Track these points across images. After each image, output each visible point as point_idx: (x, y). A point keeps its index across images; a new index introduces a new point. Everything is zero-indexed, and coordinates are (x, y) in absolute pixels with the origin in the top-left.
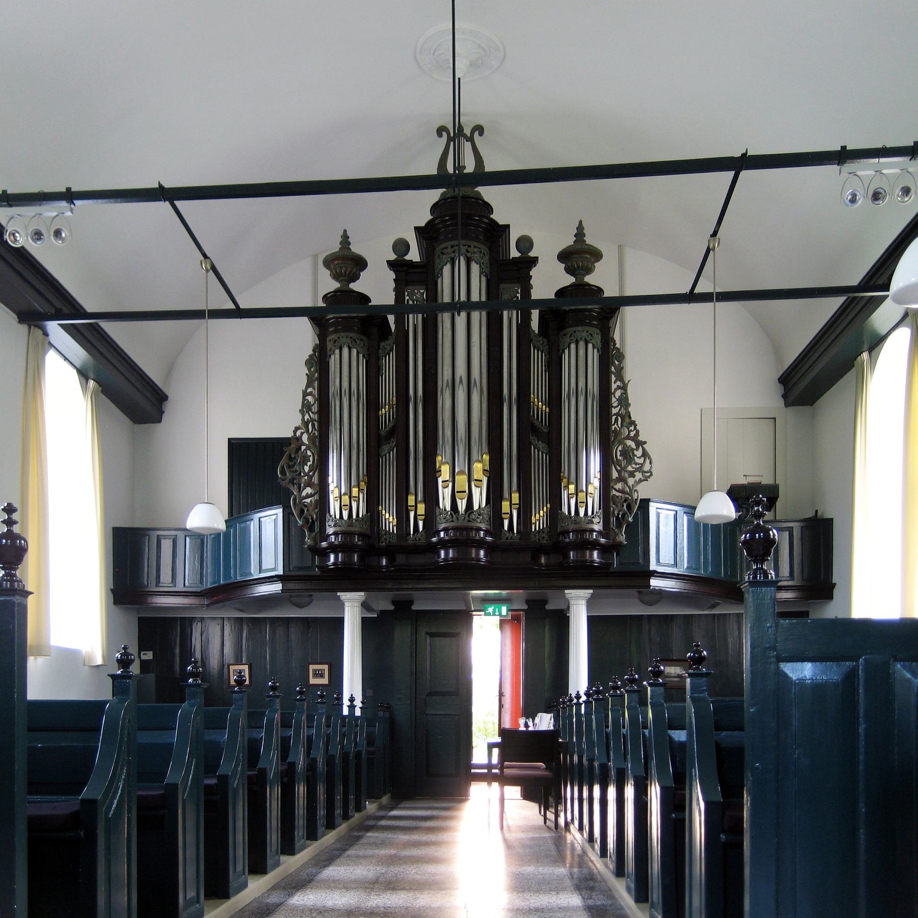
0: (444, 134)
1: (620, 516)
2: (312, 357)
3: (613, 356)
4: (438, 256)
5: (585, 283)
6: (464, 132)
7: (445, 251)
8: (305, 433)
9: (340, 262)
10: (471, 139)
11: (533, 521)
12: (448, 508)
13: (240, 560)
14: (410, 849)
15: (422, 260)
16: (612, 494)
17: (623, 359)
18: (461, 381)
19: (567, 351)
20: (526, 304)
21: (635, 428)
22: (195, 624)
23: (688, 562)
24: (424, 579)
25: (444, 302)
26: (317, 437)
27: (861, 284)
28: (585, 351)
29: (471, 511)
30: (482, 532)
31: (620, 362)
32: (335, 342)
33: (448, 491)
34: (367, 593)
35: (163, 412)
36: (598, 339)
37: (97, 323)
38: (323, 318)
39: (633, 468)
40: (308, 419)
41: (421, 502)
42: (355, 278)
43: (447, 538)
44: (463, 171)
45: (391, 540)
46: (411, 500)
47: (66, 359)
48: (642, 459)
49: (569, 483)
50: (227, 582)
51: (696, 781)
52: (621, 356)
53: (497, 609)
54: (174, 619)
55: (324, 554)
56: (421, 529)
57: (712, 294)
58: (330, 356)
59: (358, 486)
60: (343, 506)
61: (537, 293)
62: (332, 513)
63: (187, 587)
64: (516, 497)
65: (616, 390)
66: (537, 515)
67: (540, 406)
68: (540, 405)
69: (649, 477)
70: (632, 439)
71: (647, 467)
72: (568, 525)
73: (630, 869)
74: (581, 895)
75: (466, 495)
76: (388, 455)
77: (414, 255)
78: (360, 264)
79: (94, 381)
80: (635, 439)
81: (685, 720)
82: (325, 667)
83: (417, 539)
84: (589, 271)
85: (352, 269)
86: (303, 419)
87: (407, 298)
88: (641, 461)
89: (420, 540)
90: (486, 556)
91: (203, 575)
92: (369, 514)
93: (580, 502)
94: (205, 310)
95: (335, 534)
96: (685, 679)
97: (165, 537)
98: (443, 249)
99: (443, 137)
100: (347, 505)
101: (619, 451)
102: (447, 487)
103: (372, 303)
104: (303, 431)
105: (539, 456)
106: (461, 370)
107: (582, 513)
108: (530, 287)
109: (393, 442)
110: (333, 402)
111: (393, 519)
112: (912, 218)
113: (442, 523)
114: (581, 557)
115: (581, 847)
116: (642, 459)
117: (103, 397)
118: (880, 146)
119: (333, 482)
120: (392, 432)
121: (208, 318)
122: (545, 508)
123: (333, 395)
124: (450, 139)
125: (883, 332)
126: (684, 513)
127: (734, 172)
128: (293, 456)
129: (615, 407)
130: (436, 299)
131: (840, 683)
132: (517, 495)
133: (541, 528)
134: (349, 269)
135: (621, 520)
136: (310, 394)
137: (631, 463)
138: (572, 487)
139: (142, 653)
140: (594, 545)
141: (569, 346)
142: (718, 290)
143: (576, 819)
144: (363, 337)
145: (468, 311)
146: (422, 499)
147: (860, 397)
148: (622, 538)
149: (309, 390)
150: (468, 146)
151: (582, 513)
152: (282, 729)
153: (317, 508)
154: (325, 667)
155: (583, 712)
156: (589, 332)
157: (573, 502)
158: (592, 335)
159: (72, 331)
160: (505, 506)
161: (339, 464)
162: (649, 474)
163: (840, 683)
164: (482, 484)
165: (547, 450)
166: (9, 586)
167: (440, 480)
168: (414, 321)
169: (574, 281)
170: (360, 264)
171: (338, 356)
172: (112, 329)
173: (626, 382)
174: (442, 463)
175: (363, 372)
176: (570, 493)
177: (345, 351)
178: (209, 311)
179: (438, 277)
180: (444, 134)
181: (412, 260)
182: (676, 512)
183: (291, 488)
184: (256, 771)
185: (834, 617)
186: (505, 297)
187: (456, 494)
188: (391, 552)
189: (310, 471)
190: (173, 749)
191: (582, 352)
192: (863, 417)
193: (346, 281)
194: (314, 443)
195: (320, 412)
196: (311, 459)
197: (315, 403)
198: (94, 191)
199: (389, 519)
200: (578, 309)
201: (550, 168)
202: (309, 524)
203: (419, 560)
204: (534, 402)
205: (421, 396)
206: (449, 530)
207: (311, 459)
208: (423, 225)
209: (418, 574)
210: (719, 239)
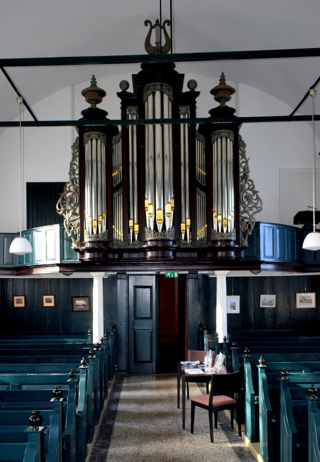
0: (149, 24)
1: (245, 231)
2: (75, 144)
3: (240, 145)
4: (145, 90)
5: (226, 106)
7: (150, 88)
11: (198, 234)
12: (152, 228)
13: (285, 245)
14: (114, 426)
15: (135, 92)
17: (245, 147)
19: (216, 143)
21: (252, 184)
22: (9, 281)
23: (280, 254)
24: (138, 265)
25: (168, 125)
26: (78, 188)
27: (189, 126)
29: (165, 230)
31: (244, 148)
32: (88, 137)
36: (232, 135)
39: (251, 205)
41: (136, 224)
42: (99, 101)
45: (120, 244)
46: (131, 223)
48: (257, 201)
49: (218, 214)
52: (244, 145)
53: (172, 274)
55: (82, 253)
56: (136, 239)
58: (85, 144)
60: (94, 226)
64: (188, 221)
65: (242, 163)
66: (200, 231)
67: (201, 172)
68: (201, 171)
69: (260, 210)
70: (251, 190)
71: (259, 205)
72: (217, 237)
73: (99, 392)
75: (162, 221)
76: (117, 198)
77: (131, 90)
78: (102, 94)
81: (35, 227)
82: (52, 297)
83: (135, 244)
84: (228, 99)
85: (98, 97)
86: (70, 178)
87: (128, 112)
88: (256, 202)
89: (136, 245)
91: (212, 425)
92: (108, 230)
93: (224, 225)
94: (19, 122)
97: (269, 257)
98: (148, 87)
99: (148, 26)
100: (162, 220)
101: (244, 196)
102: (151, 217)
104: (70, 184)
109: (121, 191)
110: (87, 164)
111: (121, 233)
113: (149, 237)
114: (19, 263)
118: (121, 110)
124: (152, 27)
126: (277, 228)
129: (241, 173)
132: (138, 226)
133: (202, 238)
134: (96, 97)
135: (245, 234)
137: (251, 203)
141: (217, 140)
143: (229, 162)
144: (104, 134)
145: (153, 124)
146: (137, 223)
147: (224, 319)
148: (246, 243)
153: (79, 227)
154: (52, 297)
155: (67, 343)
156: (228, 133)
158: (229, 134)
160: (183, 226)
161: (91, 192)
164: (171, 215)
165: (204, 195)
167: (147, 213)
168: (133, 130)
169: (220, 105)
170: (102, 94)
171: (90, 144)
172: (297, 114)
173: (247, 159)
175: (230, 149)
176: (218, 220)
177: (94, 141)
178: (22, 122)
179: (145, 102)
180: (149, 24)
182: (273, 228)
184: (94, 246)
187: (157, 221)
189: (75, 206)
192: (220, 202)
193: (94, 103)
194: (77, 192)
196: (75, 199)
197: (77, 169)
199: (119, 233)
201: (269, 294)
202: (74, 236)
204: (197, 170)
205: (220, 160)
208: (137, 73)
209: (135, 263)
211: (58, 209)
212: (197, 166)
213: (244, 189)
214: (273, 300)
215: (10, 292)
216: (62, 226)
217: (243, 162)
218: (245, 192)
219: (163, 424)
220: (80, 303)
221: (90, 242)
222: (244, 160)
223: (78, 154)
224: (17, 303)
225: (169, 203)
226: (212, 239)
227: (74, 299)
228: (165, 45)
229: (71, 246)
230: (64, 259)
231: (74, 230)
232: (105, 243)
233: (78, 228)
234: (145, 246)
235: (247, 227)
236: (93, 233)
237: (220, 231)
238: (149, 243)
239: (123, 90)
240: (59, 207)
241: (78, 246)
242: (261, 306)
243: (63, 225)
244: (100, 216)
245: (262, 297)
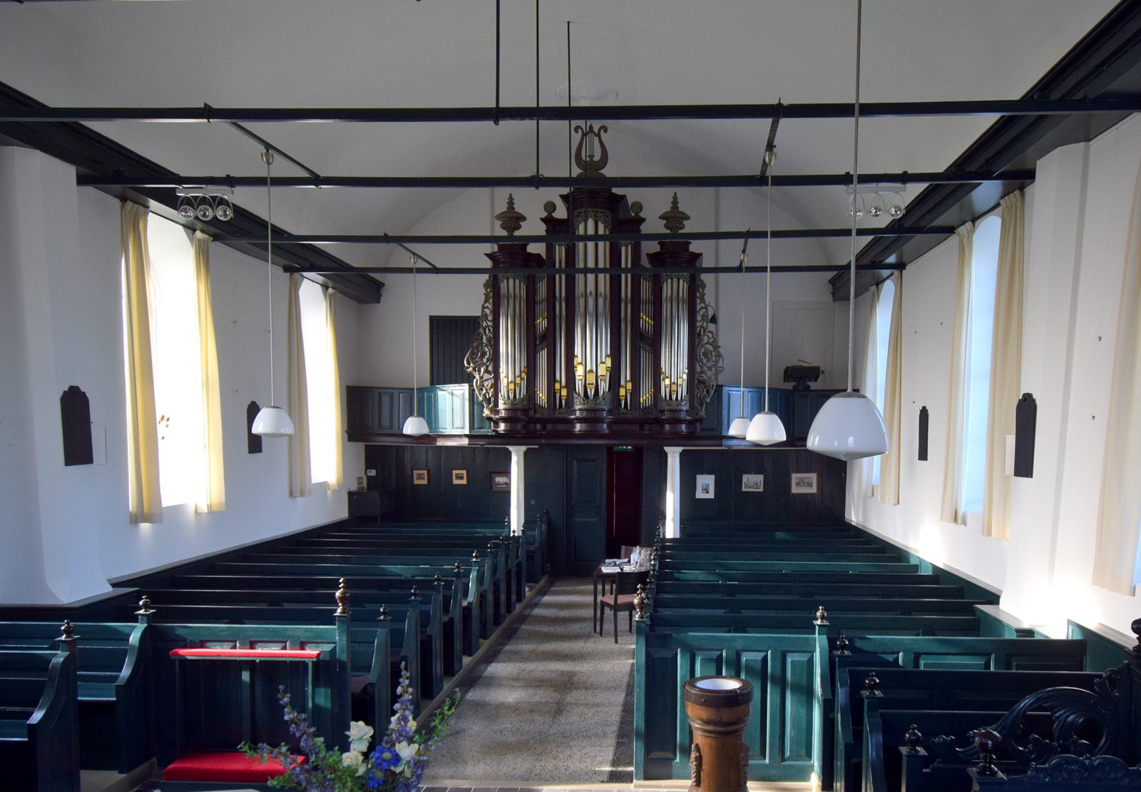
0: (580, 130)
6: (492, 122)
10: (598, 135)
14: (582, 663)
19: (665, 283)
27: (1025, 99)
28: (689, 668)
34: (1007, 181)
38: (426, 741)
44: (667, 223)
55: (496, 423)
57: (853, 106)
59: (520, 376)
69: (722, 371)
82: (464, 472)
94: (267, 178)
96: (468, 382)
103: (642, 233)
107: (674, 397)
112: (1054, 64)
120: (544, 337)
121: (772, 185)
124: (584, 135)
127: (665, 448)
129: (700, 321)
132: (621, 394)
136: (487, 307)
139: (368, 471)
142: (272, 175)
148: (703, 413)
149: (487, 305)
150: (596, 139)
151: (674, 397)
152: (821, 636)
154: (464, 472)
157: (668, 390)
163: (269, 778)
166: (816, 442)
169: (659, 250)
171: (506, 284)
177: (511, 281)
178: (413, 272)
180: (580, 130)
181: (249, 405)
183: (474, 373)
185: (501, 123)
186: (581, 232)
187: (588, 386)
188: (543, 422)
190: (371, 667)
194: (490, 343)
196: (488, 353)
199: (542, 396)
203: (560, 427)
207: (488, 353)
210: (776, 154)
211: (466, 365)
212: (642, 314)
213: (701, 344)
214: (760, 482)
215: (408, 465)
216: (471, 386)
217: (702, 308)
218: (702, 347)
219: (576, 627)
220: (500, 480)
221: (505, 409)
222: (703, 305)
223: (491, 294)
224: (418, 479)
225: (603, 363)
226: (659, 408)
227: (493, 475)
228: (601, 157)
229: (483, 412)
230: (474, 429)
231: (487, 392)
232: (525, 411)
233: (492, 390)
234: (573, 417)
235: (705, 392)
236: (508, 396)
237: (668, 398)
238: (578, 414)
239: (549, 214)
240: (469, 363)
241: (491, 412)
242: (744, 489)
243: (473, 386)
244: (518, 376)
245: (745, 477)
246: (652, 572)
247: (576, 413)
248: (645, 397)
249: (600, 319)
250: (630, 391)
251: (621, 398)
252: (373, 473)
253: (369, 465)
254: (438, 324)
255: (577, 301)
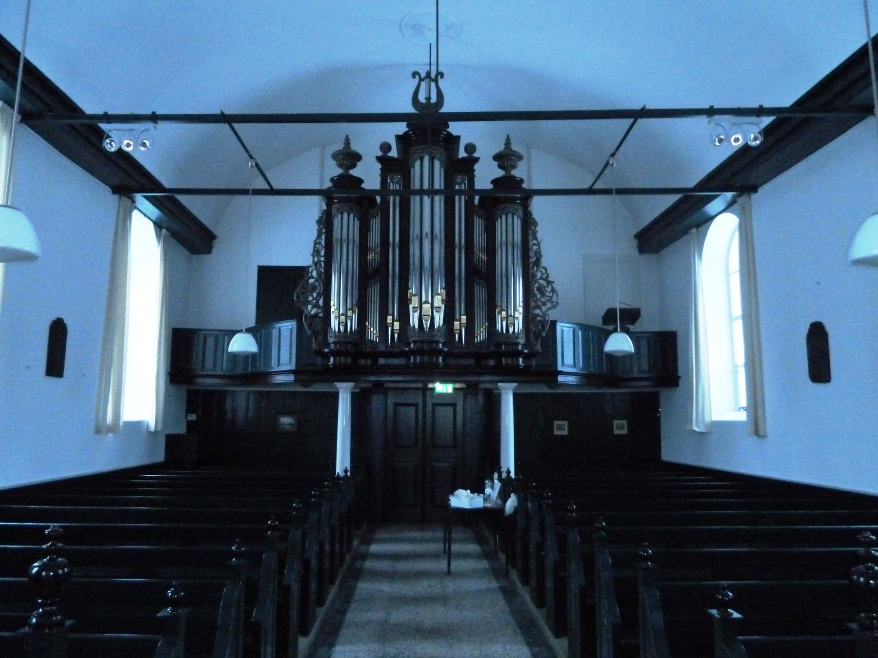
0: (417, 76)
8: (315, 270)
9: (873, 552)
16: (121, 424)
18: (344, 241)
19: (499, 220)
20: (471, 190)
21: (546, 272)
30: (441, 344)
31: (535, 227)
33: (417, 315)
35: (213, 247)
36: (520, 212)
37: (173, 195)
40: (317, 261)
42: (353, 166)
43: (415, 348)
46: (389, 319)
47: (145, 215)
48: (551, 293)
50: (626, 428)
51: (464, 419)
52: (535, 224)
54: (214, 391)
55: (326, 356)
61: (478, 186)
62: (333, 326)
63: (434, 411)
67: (480, 256)
69: (556, 306)
71: (554, 299)
74: (508, 604)
77: (394, 153)
79: (167, 230)
80: (546, 279)
82: (625, 422)
84: (514, 167)
86: (313, 261)
87: (389, 181)
88: (551, 294)
90: (523, 362)
95: (335, 343)
105: (480, 293)
106: (427, 228)
108: (474, 176)
115: (271, 374)
116: (551, 293)
117: (173, 242)
119: (334, 305)
120: (377, 271)
121: (616, 309)
122: (484, 327)
123: (440, 239)
124: (421, 80)
125: (713, 213)
128: (306, 286)
130: (409, 187)
131: (457, 386)
132: (388, 322)
138: (504, 313)
140: (439, 352)
148: (538, 347)
150: (433, 84)
157: (504, 323)
158: (517, 210)
159: (153, 201)
160: (457, 324)
162: (556, 304)
167: (411, 307)
171: (340, 218)
174: (413, 295)
177: (345, 215)
180: (417, 76)
189: (317, 296)
191: (510, 221)
195: (326, 256)
198: (624, 111)
199: (373, 332)
200: (109, 387)
206: (425, 342)
213: (535, 279)
222: (535, 242)
246: (436, 124)
247: (410, 345)
248: (481, 335)
249: (436, 276)
250: (465, 325)
251: (455, 331)
252: (193, 417)
253: (189, 411)
254: (267, 275)
255: (411, 244)
